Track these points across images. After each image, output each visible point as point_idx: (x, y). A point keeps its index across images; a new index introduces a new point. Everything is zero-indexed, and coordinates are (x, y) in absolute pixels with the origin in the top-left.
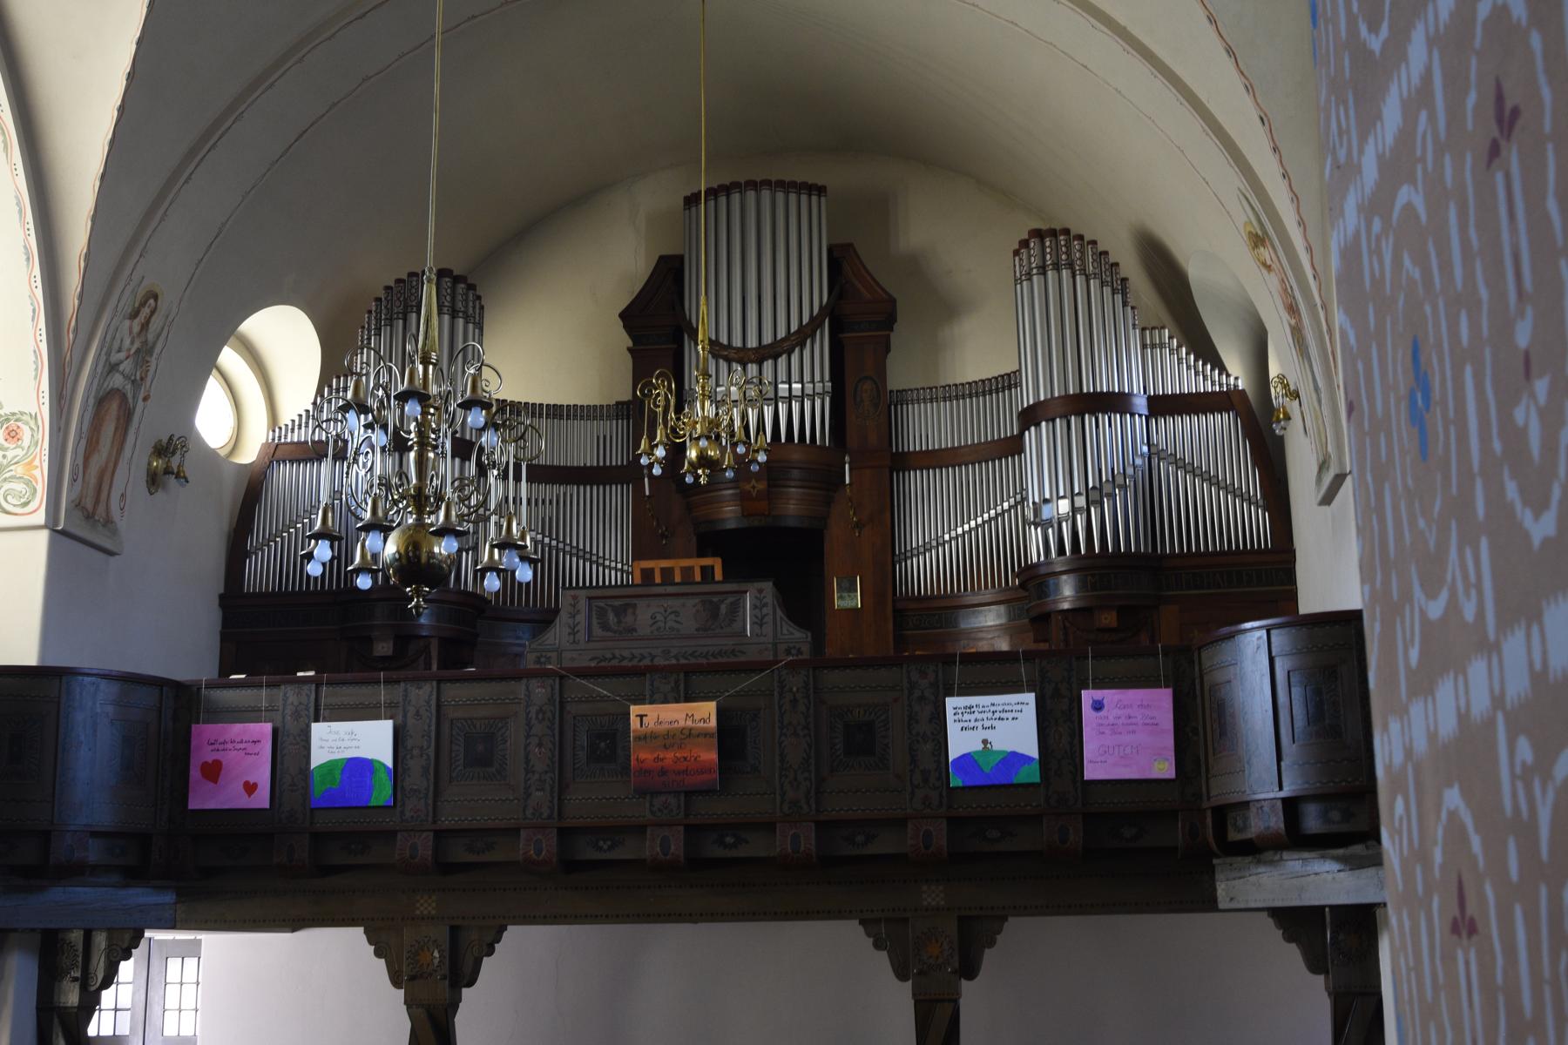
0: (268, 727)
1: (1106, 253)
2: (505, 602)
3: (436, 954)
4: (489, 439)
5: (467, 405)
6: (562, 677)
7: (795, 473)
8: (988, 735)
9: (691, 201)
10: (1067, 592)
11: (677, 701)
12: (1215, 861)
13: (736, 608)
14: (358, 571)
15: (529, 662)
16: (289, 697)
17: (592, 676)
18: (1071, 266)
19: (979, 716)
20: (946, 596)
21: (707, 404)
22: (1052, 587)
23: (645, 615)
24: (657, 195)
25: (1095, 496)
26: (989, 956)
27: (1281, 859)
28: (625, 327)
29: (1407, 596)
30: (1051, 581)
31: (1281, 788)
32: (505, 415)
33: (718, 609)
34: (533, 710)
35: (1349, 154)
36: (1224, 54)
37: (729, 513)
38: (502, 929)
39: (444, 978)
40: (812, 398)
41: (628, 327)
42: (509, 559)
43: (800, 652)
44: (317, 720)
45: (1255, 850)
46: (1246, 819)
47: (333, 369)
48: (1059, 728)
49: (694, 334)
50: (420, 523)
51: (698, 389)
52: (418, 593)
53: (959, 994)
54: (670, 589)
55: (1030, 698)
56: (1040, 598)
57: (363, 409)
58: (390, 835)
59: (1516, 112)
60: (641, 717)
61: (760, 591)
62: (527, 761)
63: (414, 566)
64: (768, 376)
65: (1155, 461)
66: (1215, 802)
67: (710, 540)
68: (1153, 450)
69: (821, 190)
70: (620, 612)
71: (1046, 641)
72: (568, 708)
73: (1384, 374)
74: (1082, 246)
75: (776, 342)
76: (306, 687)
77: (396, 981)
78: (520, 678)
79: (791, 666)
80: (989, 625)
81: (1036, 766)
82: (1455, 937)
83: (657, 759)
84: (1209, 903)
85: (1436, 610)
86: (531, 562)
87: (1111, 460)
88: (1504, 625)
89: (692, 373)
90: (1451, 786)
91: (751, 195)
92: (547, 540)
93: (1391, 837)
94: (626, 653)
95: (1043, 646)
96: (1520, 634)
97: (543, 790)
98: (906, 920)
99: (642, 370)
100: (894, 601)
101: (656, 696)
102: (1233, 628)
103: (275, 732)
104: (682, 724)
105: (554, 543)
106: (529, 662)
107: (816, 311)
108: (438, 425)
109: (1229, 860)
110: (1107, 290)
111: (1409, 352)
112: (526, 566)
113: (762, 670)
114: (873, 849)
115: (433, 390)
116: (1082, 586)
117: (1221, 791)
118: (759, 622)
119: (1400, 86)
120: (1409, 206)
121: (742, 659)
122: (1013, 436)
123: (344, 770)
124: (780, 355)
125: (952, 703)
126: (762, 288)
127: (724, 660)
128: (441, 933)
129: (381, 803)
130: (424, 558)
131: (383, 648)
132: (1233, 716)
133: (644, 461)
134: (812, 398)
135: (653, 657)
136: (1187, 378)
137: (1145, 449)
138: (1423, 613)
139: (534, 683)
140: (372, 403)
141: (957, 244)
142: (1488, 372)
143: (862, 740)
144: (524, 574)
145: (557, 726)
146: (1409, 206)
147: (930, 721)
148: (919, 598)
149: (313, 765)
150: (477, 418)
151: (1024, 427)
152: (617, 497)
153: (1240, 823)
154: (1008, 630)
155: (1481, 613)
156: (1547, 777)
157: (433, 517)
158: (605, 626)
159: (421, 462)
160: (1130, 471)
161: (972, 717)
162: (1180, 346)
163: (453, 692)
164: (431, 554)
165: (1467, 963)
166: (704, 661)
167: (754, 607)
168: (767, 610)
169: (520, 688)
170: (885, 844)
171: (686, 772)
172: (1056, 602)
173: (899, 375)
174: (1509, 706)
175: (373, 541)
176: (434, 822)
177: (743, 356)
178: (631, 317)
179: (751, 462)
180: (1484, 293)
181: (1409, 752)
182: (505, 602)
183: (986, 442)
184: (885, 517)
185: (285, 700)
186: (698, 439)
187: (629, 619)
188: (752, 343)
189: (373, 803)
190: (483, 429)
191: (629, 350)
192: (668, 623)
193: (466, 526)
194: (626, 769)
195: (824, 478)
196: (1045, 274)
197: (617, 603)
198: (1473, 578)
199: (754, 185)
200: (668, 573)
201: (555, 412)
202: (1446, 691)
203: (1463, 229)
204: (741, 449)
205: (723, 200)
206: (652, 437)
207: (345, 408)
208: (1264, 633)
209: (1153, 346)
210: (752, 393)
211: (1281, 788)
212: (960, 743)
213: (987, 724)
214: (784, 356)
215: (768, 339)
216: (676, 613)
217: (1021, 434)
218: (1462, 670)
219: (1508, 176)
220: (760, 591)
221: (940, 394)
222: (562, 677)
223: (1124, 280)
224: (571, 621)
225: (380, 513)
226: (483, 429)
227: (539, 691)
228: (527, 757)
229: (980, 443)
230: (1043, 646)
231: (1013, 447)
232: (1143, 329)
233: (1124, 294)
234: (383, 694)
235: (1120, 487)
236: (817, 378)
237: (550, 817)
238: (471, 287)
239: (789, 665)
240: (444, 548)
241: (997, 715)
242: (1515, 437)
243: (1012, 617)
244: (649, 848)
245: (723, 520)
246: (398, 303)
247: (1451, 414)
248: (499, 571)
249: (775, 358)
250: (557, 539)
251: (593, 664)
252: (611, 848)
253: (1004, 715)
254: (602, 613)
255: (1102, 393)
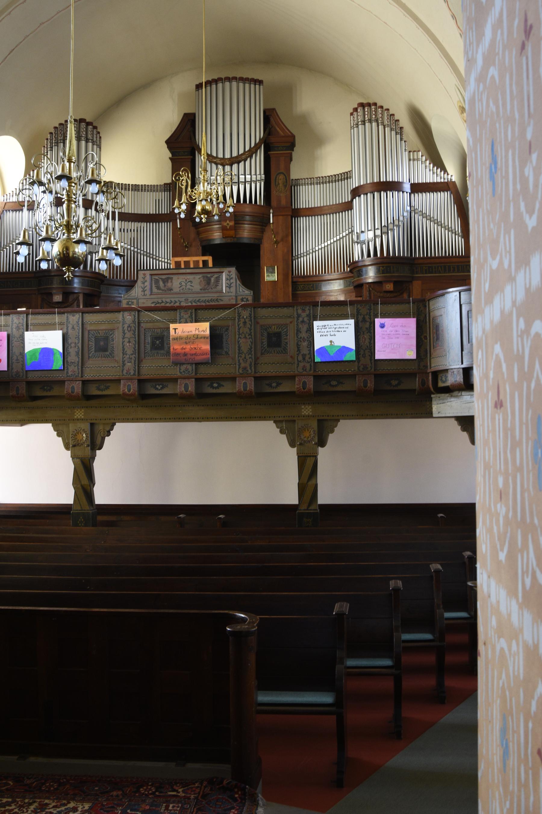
0: (5, 334)
1: (393, 115)
2: (113, 277)
3: (84, 435)
4: (100, 199)
5: (90, 182)
6: (139, 311)
7: (248, 218)
8: (332, 338)
9: (199, 87)
10: (371, 275)
11: (191, 322)
12: (432, 396)
13: (218, 280)
14: (40, 260)
15: (124, 305)
16: (15, 320)
17: (153, 311)
18: (377, 121)
19: (329, 330)
20: (316, 276)
21: (206, 184)
22: (364, 272)
23: (176, 283)
24: (184, 83)
25: (385, 230)
26: (331, 437)
27: (461, 395)
28: (168, 147)
29: (486, 260)
30: (364, 269)
31: (462, 363)
32: (107, 187)
33: (210, 280)
34: (126, 326)
35: (473, 54)
36: (451, 18)
37: (217, 237)
38: (114, 424)
39: (88, 446)
40: (256, 182)
41: (170, 148)
42: (110, 255)
43: (247, 300)
44: (27, 330)
45: (448, 390)
46: (446, 377)
47: (32, 166)
48: (365, 335)
49: (200, 151)
50: (69, 238)
51: (201, 177)
52: (68, 270)
53: (317, 453)
54: (188, 271)
55: (352, 322)
56: (359, 277)
57: (41, 184)
58: (62, 383)
59: (531, 27)
60: (175, 329)
61: (230, 272)
62: (124, 350)
63: (67, 259)
64: (235, 171)
65: (413, 214)
66: (433, 369)
67: (208, 249)
68: (412, 209)
69: (260, 82)
70: (165, 281)
71: (361, 297)
72: (142, 325)
73: (481, 158)
74: (382, 111)
75: (239, 156)
76: (22, 315)
77: (67, 447)
78: (120, 312)
79: (244, 306)
80: (335, 289)
81: (354, 353)
82: (496, 409)
83: (183, 348)
84: (429, 414)
85: (495, 264)
86: (121, 256)
87: (393, 214)
88: (518, 269)
89: (199, 169)
90: (496, 343)
91: (227, 84)
92: (132, 248)
93: (477, 369)
94: (168, 300)
95: (359, 299)
96: (522, 271)
97: (131, 362)
98: (294, 421)
99: (175, 170)
100: (292, 278)
101: (182, 320)
102: (444, 291)
103: (8, 336)
104: (194, 333)
105: (136, 250)
106: (124, 305)
107: (258, 141)
108: (76, 192)
109: (438, 395)
110: (393, 133)
111: (490, 147)
112: (118, 258)
113: (230, 308)
114: (280, 389)
115: (74, 175)
116: (378, 271)
117: (436, 364)
118: (229, 286)
119: (491, 19)
120: (493, 77)
121: (221, 303)
122: (348, 202)
123: (40, 353)
124: (240, 162)
125: (316, 324)
126: (232, 129)
127: (213, 303)
128: (86, 426)
129: (58, 368)
130: (71, 254)
131: (58, 298)
132: (442, 331)
133: (176, 211)
134: (256, 182)
135: (180, 302)
136: (429, 175)
137: (409, 208)
138: (490, 266)
139: (126, 314)
140: (45, 180)
141: (323, 109)
142: (517, 152)
143: (275, 340)
144: (117, 262)
145: (137, 333)
146: (493, 77)
147: (307, 332)
148: (302, 277)
149: (26, 351)
150: (94, 188)
151: (353, 197)
152: (165, 228)
153: (444, 379)
154: (343, 291)
155: (510, 265)
156: (528, 334)
157: (75, 235)
158: (158, 288)
159: (69, 209)
160: (401, 218)
161: (326, 330)
162: (426, 160)
163: (89, 318)
164: (74, 253)
165: (499, 420)
166: (204, 304)
167: (227, 279)
168: (233, 281)
169: (120, 316)
170: (285, 387)
171: (195, 354)
172: (366, 278)
173: (297, 171)
174: (517, 305)
175: (46, 246)
176: (82, 377)
177: (223, 162)
178: (171, 143)
179: (226, 212)
180: (517, 116)
181: (484, 331)
182: (113, 277)
183: (336, 204)
184: (289, 238)
185: (12, 321)
186: (201, 200)
187: (169, 284)
188: (228, 156)
189: (54, 368)
190: (97, 194)
191: (170, 158)
192: (187, 287)
193: (89, 239)
194: (168, 352)
195: (261, 221)
196: (364, 124)
197: (164, 277)
198: (508, 249)
199: (228, 79)
200: (187, 263)
201: (136, 188)
202: (497, 301)
203: (511, 85)
204: (221, 206)
205: (214, 86)
206: (180, 200)
207: (32, 184)
208: (458, 293)
209: (414, 160)
210: (227, 179)
211: (462, 363)
212: (319, 342)
213: (332, 333)
214: (243, 162)
215: (235, 154)
216: (191, 282)
217: (352, 200)
218: (502, 291)
219: (527, 58)
220: (230, 272)
221: (315, 182)
222: (139, 311)
223: (401, 128)
224: (142, 285)
225: (50, 233)
226: (97, 194)
227: (129, 318)
228: (123, 347)
229: (333, 205)
230: (359, 299)
231: (348, 206)
232: (410, 152)
233: (401, 135)
234: (57, 318)
235: (396, 226)
236: (258, 173)
237: (134, 374)
238: (95, 128)
239: (242, 306)
240: (80, 249)
241: (337, 330)
242: (524, 180)
243: (346, 285)
244: (179, 389)
245: (214, 240)
246: (58, 135)
247: (504, 174)
248: (106, 261)
249: (238, 163)
250: (137, 248)
251: (153, 305)
252: (162, 388)
253: (340, 330)
254: (157, 282)
255: (389, 182)
